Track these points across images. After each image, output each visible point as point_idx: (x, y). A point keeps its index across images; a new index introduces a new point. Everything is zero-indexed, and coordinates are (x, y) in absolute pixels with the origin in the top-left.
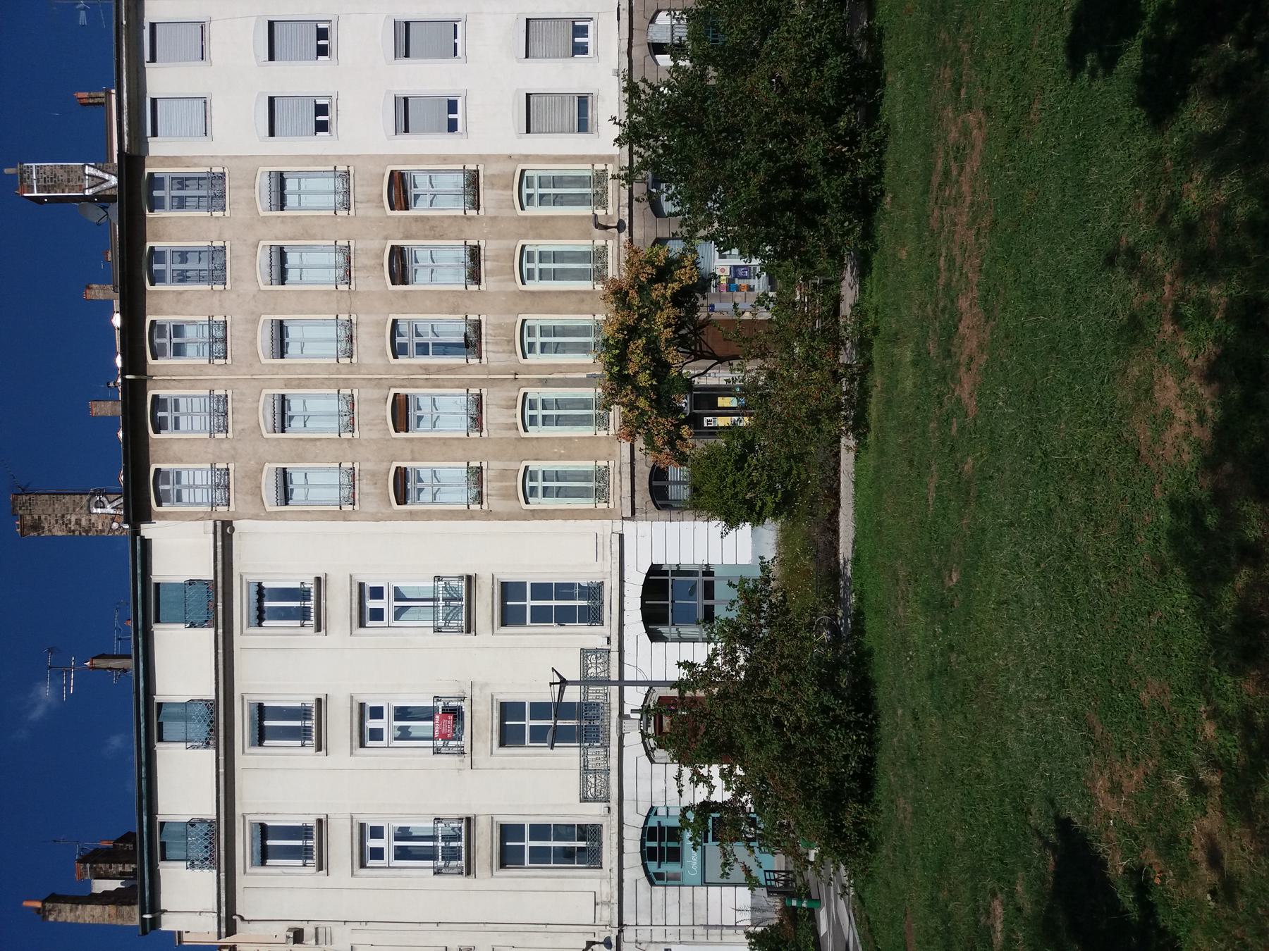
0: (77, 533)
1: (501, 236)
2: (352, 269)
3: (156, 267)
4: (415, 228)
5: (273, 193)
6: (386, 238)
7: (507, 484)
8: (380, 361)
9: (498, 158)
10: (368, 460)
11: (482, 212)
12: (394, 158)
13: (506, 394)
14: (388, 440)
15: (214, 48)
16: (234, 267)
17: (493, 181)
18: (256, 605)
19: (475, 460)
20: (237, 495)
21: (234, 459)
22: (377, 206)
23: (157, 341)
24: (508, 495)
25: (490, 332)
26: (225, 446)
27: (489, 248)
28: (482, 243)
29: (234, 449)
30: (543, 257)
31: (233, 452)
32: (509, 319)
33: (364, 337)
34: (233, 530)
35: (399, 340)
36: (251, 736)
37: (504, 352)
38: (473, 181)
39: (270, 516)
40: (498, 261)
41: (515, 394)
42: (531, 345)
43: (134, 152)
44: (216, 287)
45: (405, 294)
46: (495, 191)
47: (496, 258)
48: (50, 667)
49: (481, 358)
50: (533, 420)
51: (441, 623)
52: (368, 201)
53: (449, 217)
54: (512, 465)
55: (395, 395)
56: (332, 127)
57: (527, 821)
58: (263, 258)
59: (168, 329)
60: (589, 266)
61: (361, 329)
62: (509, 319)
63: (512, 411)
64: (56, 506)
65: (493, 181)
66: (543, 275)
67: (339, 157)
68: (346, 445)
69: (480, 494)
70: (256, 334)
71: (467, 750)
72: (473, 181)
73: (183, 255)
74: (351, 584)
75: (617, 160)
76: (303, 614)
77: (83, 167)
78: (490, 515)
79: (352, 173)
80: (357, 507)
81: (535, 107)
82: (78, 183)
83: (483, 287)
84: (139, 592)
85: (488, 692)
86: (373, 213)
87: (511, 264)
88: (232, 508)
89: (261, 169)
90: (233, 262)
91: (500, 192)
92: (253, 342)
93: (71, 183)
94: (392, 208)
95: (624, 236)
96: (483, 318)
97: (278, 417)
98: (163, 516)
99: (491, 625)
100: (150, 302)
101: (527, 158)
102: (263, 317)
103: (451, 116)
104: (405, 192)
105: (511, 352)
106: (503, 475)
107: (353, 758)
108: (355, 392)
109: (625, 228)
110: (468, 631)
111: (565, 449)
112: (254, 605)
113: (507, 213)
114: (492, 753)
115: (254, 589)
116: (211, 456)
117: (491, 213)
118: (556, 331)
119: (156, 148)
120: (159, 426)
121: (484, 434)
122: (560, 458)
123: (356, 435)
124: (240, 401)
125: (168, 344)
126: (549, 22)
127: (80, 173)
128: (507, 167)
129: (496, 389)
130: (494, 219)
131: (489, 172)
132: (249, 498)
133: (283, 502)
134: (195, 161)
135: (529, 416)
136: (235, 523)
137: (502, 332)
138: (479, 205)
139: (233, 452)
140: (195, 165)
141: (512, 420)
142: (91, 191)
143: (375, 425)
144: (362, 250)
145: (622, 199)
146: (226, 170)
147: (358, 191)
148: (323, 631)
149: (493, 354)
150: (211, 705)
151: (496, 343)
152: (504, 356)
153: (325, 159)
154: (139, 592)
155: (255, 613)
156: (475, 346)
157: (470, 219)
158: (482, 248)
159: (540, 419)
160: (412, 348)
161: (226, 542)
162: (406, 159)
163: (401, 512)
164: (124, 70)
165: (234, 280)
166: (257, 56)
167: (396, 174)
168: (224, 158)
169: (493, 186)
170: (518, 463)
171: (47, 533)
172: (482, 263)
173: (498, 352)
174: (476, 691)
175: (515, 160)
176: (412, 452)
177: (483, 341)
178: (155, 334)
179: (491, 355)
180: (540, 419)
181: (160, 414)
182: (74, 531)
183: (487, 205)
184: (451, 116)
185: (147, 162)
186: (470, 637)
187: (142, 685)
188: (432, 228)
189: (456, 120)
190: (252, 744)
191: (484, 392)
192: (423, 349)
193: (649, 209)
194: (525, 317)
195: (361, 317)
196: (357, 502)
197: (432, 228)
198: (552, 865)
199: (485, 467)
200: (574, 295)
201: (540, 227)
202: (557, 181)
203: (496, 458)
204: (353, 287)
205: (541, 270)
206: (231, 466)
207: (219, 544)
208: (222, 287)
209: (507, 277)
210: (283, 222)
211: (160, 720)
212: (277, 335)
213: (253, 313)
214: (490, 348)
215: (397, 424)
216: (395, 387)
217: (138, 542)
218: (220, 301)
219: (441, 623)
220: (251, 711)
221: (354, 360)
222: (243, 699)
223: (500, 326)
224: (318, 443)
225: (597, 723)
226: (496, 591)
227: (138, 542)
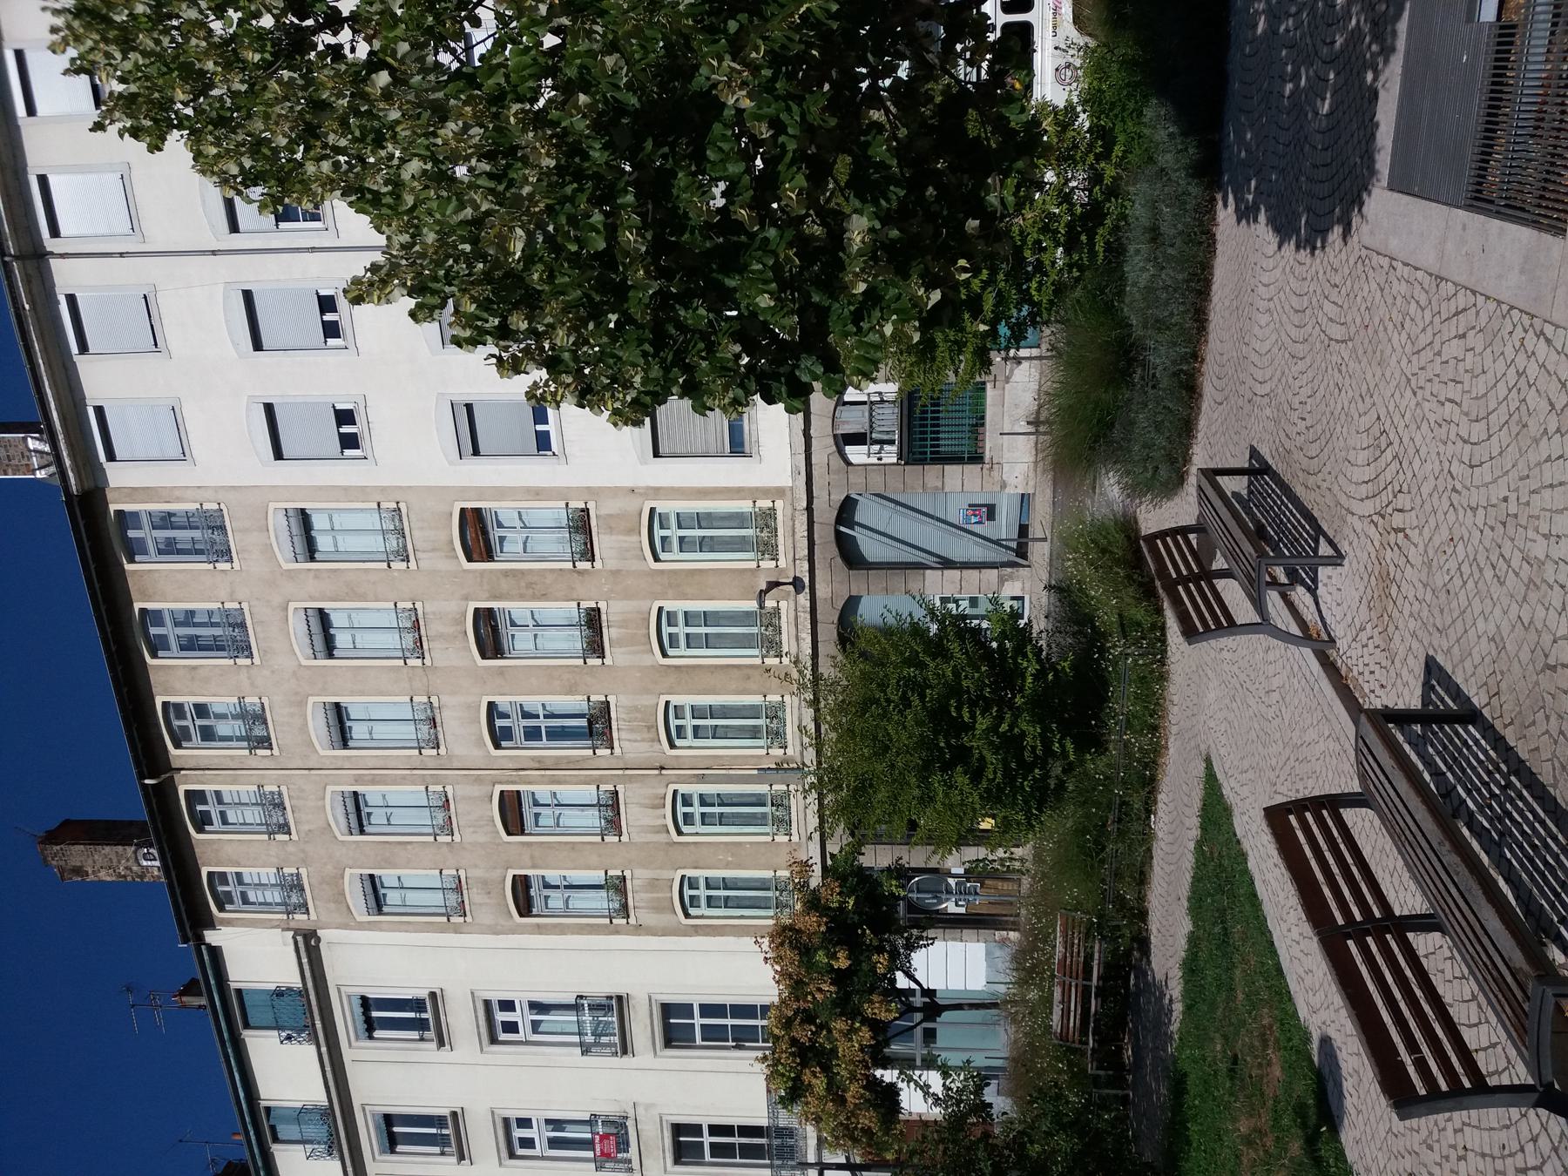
0: (129, 879)
1: (627, 595)
2: (424, 639)
3: (153, 631)
4: (505, 585)
5: (291, 519)
6: (467, 598)
7: (660, 895)
8: (477, 752)
9: (615, 491)
10: (476, 866)
11: (598, 564)
12: (463, 491)
13: (650, 791)
14: (499, 845)
15: (171, 332)
16: (260, 635)
17: (611, 523)
18: (362, 1018)
19: (616, 868)
20: (317, 903)
21: (305, 862)
22: (447, 557)
23: (176, 723)
24: (663, 907)
25: (623, 716)
26: (291, 848)
27: (612, 612)
28: (602, 605)
29: (303, 851)
30: (689, 618)
31: (302, 855)
32: (647, 700)
33: (451, 724)
34: (318, 940)
35: (499, 723)
36: (380, 1144)
37: (643, 740)
38: (581, 524)
39: (361, 926)
40: (626, 628)
41: (662, 791)
42: (680, 729)
43: (88, 485)
44: (240, 661)
45: (501, 671)
46: (614, 537)
47: (624, 624)
48: (133, 1006)
49: (612, 748)
50: (688, 819)
51: (590, 1039)
52: (434, 550)
53: (552, 570)
54: (666, 874)
55: (502, 792)
56: (365, 442)
57: (706, 1124)
58: (297, 625)
59: (187, 709)
60: (755, 630)
61: (446, 714)
62: (647, 700)
63: (661, 812)
64: (96, 857)
65: (611, 523)
66: (691, 641)
67: (383, 489)
68: (445, 849)
69: (625, 907)
70: (306, 719)
71: (635, 1164)
72: (581, 524)
73: (189, 618)
74: (474, 1002)
75: (788, 493)
76: (421, 1025)
77: (25, 439)
78: (639, 929)
79: (404, 511)
80: (469, 919)
81: (665, 430)
82: (24, 462)
83: (608, 661)
84: (218, 1003)
85: (655, 1112)
86: (444, 565)
87: (645, 631)
88: (313, 916)
89: (272, 506)
90: (258, 629)
91: (622, 538)
92: (304, 728)
93: (13, 462)
94: (470, 559)
95: (804, 599)
96: (612, 699)
97: (353, 818)
98: (228, 923)
99: (650, 1042)
100: (154, 678)
101: (657, 492)
102: (311, 700)
103: (540, 428)
104: (485, 532)
105: (653, 741)
106: (653, 884)
107: (502, 1169)
108: (449, 789)
109: (804, 588)
110: (625, 1052)
111: (733, 855)
112: (360, 1019)
113: (635, 565)
114: (665, 1171)
115: (357, 1003)
116: (275, 860)
117: (612, 564)
118: (713, 712)
119: (118, 476)
120: (202, 822)
121: (625, 838)
122: (727, 866)
123: (457, 838)
124: (298, 798)
125: (192, 728)
126: (683, 451)
127: (21, 447)
128: (630, 505)
129: (635, 785)
130: (616, 573)
131: (603, 512)
132: (332, 906)
133: (375, 910)
134: (177, 493)
135: (682, 813)
136: (320, 933)
137: (639, 715)
138: (593, 555)
139: (302, 855)
140: (178, 500)
141: (660, 822)
142: (43, 472)
143: (481, 826)
144: (434, 613)
145: (798, 550)
146: (222, 506)
147: (418, 536)
148: (448, 1047)
149: (628, 742)
150: (327, 1114)
151: (632, 730)
152: (644, 746)
153: (362, 492)
154: (218, 1003)
155: (362, 1026)
156: (603, 734)
157: (582, 573)
158: (603, 611)
159: (697, 818)
160: (518, 733)
161: (313, 956)
162: (481, 492)
163: (525, 925)
164: (45, 378)
165: (264, 653)
166: (236, 345)
167: (469, 516)
168: (217, 489)
169: (611, 530)
170: (672, 872)
171: (91, 878)
172: (605, 630)
173: (636, 741)
174: (640, 1111)
175: (641, 494)
176: (532, 857)
177: (614, 727)
178: (172, 716)
179: (625, 744)
180: (697, 818)
181: (199, 808)
182: (125, 876)
183: (604, 556)
184: (540, 428)
185: (110, 496)
186: (625, 1058)
187: (242, 1095)
188: (530, 585)
189: (547, 433)
190: (383, 1152)
191: (620, 788)
192: (532, 734)
193: (839, 560)
194: (668, 698)
195: (444, 698)
196: (468, 913)
197: (533, 588)
198: (738, 1160)
199: (628, 876)
200: (735, 670)
201: (679, 583)
202: (702, 520)
203: (644, 867)
204: (428, 661)
205: (687, 635)
206: (303, 871)
207: (305, 960)
208: (248, 661)
209: (641, 648)
210: (316, 577)
211: (272, 1123)
212: (333, 721)
213: (297, 693)
214: (624, 735)
215: (510, 825)
216: (501, 783)
217: (205, 952)
218: (249, 678)
219: (590, 1039)
220: (377, 1127)
221: (442, 751)
222: (364, 1110)
223: (636, 709)
224: (409, 847)
225: (791, 1142)
226: (655, 1012)
227: (205, 952)
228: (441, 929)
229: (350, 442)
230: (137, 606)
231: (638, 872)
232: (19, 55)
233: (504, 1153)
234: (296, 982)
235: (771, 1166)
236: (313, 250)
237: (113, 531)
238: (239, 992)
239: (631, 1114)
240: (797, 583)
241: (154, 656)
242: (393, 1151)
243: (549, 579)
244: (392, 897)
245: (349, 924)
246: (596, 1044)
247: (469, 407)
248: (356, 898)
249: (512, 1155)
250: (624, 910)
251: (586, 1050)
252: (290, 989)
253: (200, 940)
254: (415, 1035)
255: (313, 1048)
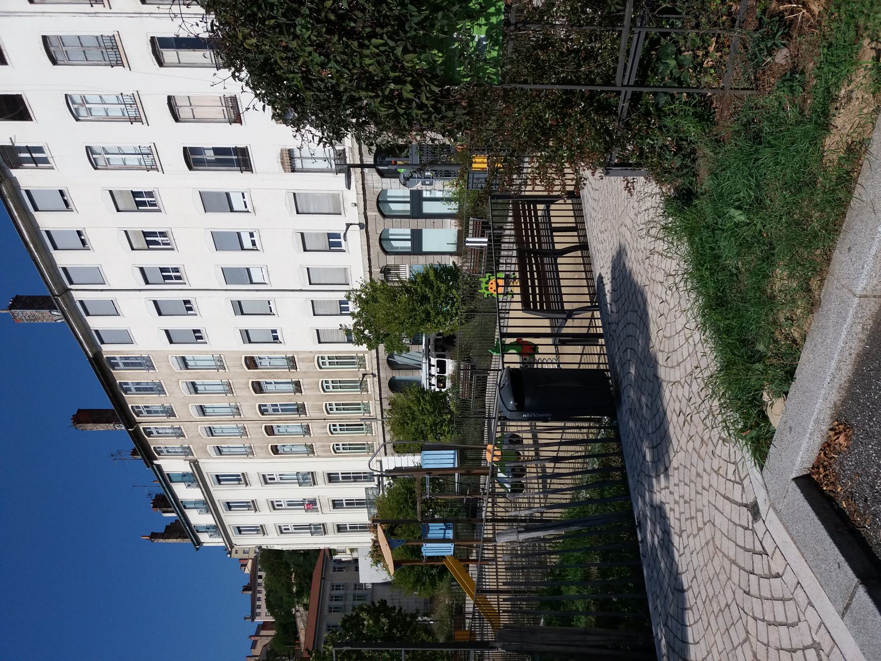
1: (310, 377)
4: (263, 375)
6: (249, 378)
21: (191, 444)
28: (301, 380)
39: (214, 458)
51: (301, 481)
78: (318, 456)
86: (239, 370)
88: (195, 456)
95: (376, 379)
102: (190, 405)
115: (215, 478)
128: (311, 355)
150: (205, 503)
153: (206, 353)
168: (147, 351)
174: (321, 498)
195: (242, 403)
201: (328, 374)
202: (337, 358)
204: (235, 394)
219: (301, 481)
228: (245, 458)
229: (190, 309)
230: (118, 382)
231: (309, 403)
232: (28, 192)
233: (272, 509)
234: (213, 523)
235: (367, 508)
236: (181, 290)
237: (106, 363)
238: (168, 474)
239: (317, 498)
240: (374, 375)
241: (114, 369)
242: (230, 510)
243: (280, 374)
244: (199, 388)
245: (209, 457)
246: (304, 483)
247: (247, 331)
248: (213, 453)
249: (282, 533)
250: (313, 453)
251: (300, 484)
252: (211, 526)
253: (153, 464)
254: (237, 482)
255: (199, 489)
